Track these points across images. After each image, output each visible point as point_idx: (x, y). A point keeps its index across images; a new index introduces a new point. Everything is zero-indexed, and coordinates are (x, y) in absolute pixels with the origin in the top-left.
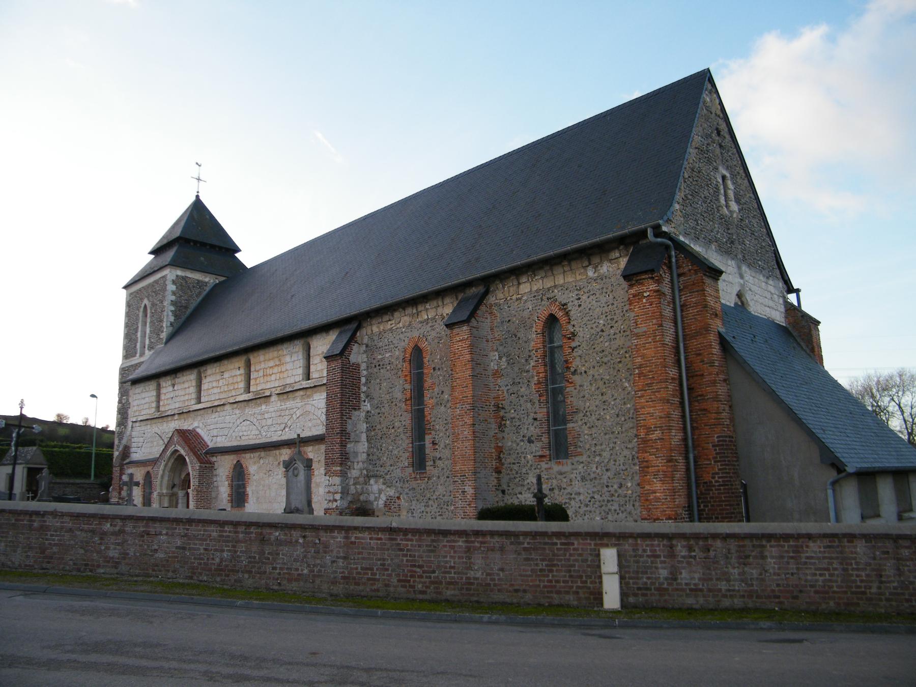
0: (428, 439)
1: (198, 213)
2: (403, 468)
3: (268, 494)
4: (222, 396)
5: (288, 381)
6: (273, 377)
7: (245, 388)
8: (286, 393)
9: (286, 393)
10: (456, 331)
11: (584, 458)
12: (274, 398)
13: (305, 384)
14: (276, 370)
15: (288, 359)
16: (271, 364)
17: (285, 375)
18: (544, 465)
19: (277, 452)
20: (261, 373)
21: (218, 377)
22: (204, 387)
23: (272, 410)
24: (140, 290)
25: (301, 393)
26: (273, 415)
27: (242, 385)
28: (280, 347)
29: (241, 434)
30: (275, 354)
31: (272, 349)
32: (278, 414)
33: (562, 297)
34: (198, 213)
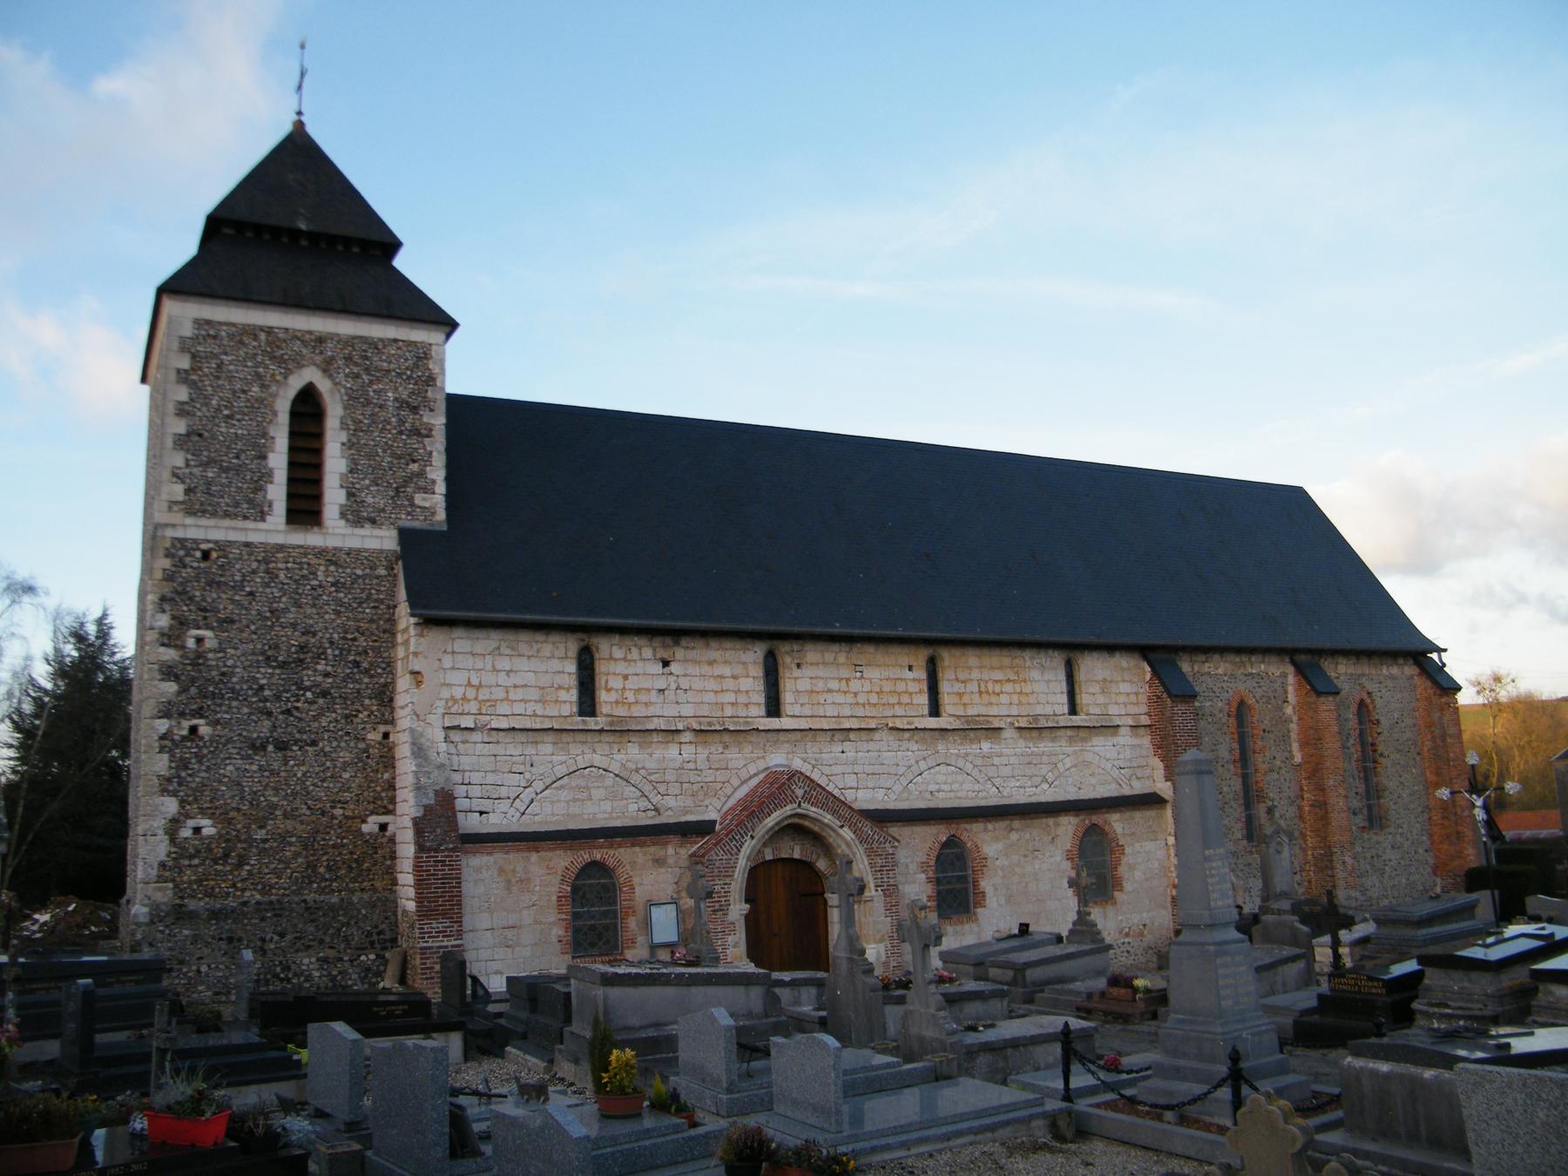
0: (1261, 810)
1: (298, 158)
2: (1236, 842)
3: (1026, 886)
4: (869, 712)
5: (1039, 710)
6: (1004, 699)
7: (581, 703)
8: (1034, 729)
9: (1034, 729)
10: (1322, 699)
11: (1392, 830)
12: (1123, 731)
13: (933, 723)
14: (1008, 687)
15: (1035, 674)
16: (998, 675)
17: (1032, 699)
18: (1366, 836)
19: (1051, 821)
20: (973, 687)
21: (845, 673)
22: (945, 687)
23: (1011, 751)
24: (321, 340)
25: (1069, 732)
26: (1013, 760)
27: (924, 699)
28: (986, 651)
29: (932, 787)
30: (1006, 661)
31: (997, 651)
32: (1027, 759)
33: (1371, 686)
34: (298, 158)
